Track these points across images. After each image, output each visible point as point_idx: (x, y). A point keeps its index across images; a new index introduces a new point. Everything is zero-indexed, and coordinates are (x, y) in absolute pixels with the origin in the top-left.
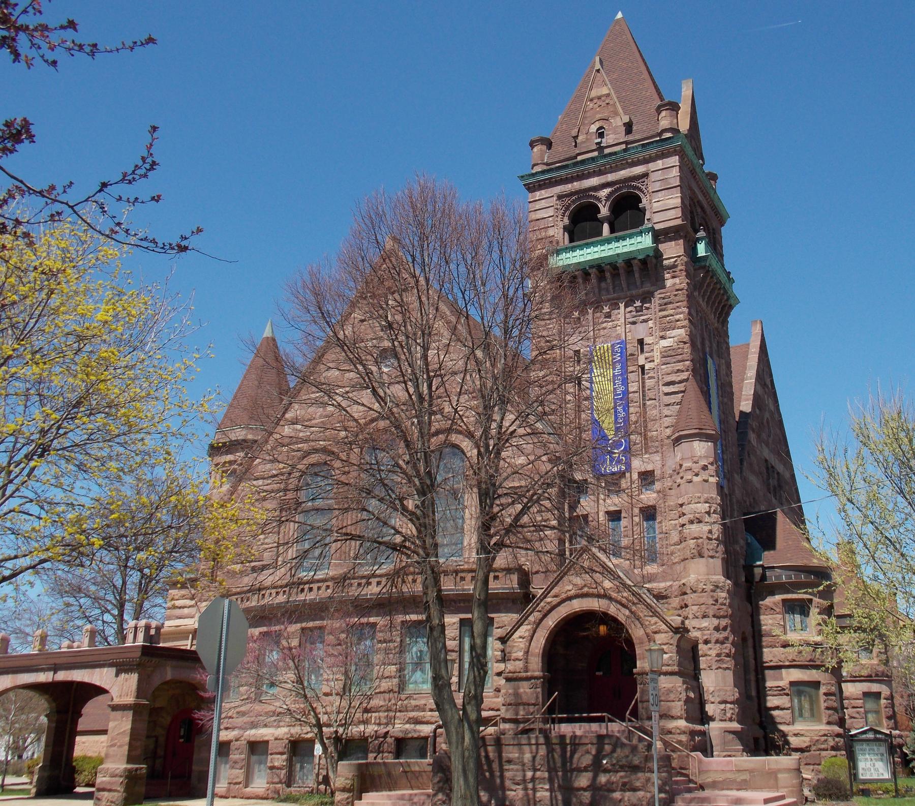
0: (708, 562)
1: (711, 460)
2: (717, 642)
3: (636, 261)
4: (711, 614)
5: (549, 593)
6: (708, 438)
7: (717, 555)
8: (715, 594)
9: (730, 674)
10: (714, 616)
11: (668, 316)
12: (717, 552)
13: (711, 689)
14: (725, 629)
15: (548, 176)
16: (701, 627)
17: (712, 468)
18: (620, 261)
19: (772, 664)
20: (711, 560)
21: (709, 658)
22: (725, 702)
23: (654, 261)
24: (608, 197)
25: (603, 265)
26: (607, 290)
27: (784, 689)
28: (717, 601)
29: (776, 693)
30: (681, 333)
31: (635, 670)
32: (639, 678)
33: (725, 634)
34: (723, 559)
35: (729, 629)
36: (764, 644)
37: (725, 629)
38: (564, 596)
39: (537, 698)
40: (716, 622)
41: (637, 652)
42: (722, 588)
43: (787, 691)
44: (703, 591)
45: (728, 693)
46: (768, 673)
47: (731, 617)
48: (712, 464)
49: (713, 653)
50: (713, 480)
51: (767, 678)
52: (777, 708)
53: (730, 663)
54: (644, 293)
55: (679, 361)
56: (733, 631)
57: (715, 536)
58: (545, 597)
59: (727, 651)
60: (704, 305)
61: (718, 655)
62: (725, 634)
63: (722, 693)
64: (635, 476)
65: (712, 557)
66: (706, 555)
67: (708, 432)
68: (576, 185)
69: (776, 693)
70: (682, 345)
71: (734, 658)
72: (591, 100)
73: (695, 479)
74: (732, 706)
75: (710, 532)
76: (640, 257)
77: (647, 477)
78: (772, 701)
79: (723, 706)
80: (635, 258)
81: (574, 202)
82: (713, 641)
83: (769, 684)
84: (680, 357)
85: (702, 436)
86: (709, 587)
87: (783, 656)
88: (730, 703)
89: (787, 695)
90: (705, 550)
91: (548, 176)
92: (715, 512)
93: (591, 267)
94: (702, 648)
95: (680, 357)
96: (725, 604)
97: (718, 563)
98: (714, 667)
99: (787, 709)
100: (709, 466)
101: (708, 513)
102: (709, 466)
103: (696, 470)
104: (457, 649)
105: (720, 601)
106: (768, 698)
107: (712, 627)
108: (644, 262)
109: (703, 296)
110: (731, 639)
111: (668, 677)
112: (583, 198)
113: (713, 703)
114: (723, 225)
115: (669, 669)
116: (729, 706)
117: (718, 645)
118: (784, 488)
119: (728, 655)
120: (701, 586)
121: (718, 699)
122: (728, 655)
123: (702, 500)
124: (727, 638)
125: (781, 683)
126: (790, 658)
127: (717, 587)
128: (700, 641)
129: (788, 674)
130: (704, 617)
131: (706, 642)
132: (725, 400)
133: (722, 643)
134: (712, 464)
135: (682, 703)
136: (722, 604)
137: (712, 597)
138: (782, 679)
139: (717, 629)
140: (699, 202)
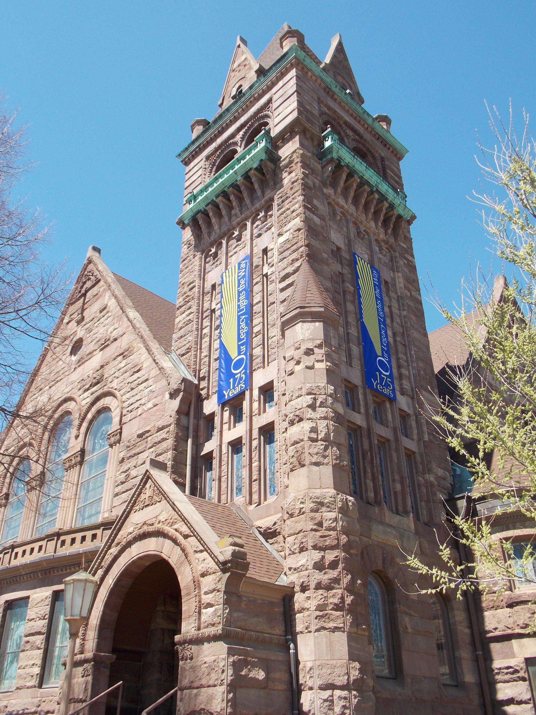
0: (310, 471)
1: (319, 342)
2: (318, 586)
3: (252, 171)
4: (310, 544)
5: (113, 541)
6: (314, 317)
7: (326, 461)
8: (317, 515)
9: (341, 639)
10: (315, 547)
11: (285, 212)
12: (325, 457)
13: (309, 665)
14: (333, 565)
15: (197, 144)
16: (294, 565)
17: (320, 353)
18: (239, 178)
19: (497, 633)
20: (315, 468)
21: (306, 613)
22: (331, 687)
23: (270, 165)
24: (242, 138)
25: (226, 189)
26: (236, 215)
27: (516, 671)
28: (320, 524)
29: (507, 677)
30: (297, 222)
31: (177, 638)
32: (180, 648)
33: (333, 574)
34: (334, 466)
35: (341, 566)
36: (484, 605)
37: (333, 565)
38: (124, 543)
39: (86, 690)
40: (317, 555)
41: (183, 609)
42: (329, 506)
43: (521, 674)
44: (301, 512)
45: (337, 671)
46: (495, 647)
47: (347, 548)
48: (320, 346)
49: (312, 604)
50: (322, 366)
51: (495, 655)
52: (511, 701)
53: (340, 619)
54: (267, 202)
55: (294, 251)
56: (348, 569)
57: (322, 436)
58: (110, 548)
59: (336, 601)
60: (352, 209)
61: (320, 608)
62: (333, 574)
63: (326, 671)
64: (256, 392)
65: (317, 464)
66: (307, 462)
67: (313, 309)
68: (219, 141)
69: (507, 677)
70: (296, 234)
71: (350, 611)
72: (234, 71)
73: (298, 368)
74: (345, 693)
75: (314, 430)
76: (255, 166)
77: (267, 391)
78: (504, 691)
79: (327, 694)
80: (251, 169)
81: (218, 157)
82: (312, 585)
83: (497, 664)
84: (294, 247)
85: (304, 315)
86: (309, 505)
87: (511, 620)
88: (342, 688)
89: (523, 679)
90: (306, 454)
91: (197, 144)
92: (322, 405)
93: (217, 197)
94: (299, 599)
95: (294, 247)
96: (334, 529)
97: (327, 473)
98: (313, 628)
99: (526, 702)
100: (316, 350)
101: (312, 407)
102: (316, 350)
103: (296, 358)
104: (44, 630)
105: (325, 524)
106: (499, 686)
107: (311, 564)
108: (260, 169)
109: (346, 197)
110: (346, 579)
111: (212, 644)
112: (225, 149)
113: (311, 689)
114: (400, 159)
115: (212, 631)
116: (338, 693)
117: (321, 592)
118: (287, 285)
119: (337, 608)
120: (299, 506)
121: (319, 682)
122: (337, 608)
123: (304, 391)
124: (336, 580)
125: (512, 662)
126: (521, 623)
127: (322, 504)
128: (297, 588)
129: (521, 647)
130: (302, 550)
131: (304, 588)
132: (405, 313)
133: (329, 588)
134: (320, 346)
135: (223, 688)
136: (329, 529)
137: (312, 519)
138: (513, 656)
139: (319, 566)
140: (346, 123)
